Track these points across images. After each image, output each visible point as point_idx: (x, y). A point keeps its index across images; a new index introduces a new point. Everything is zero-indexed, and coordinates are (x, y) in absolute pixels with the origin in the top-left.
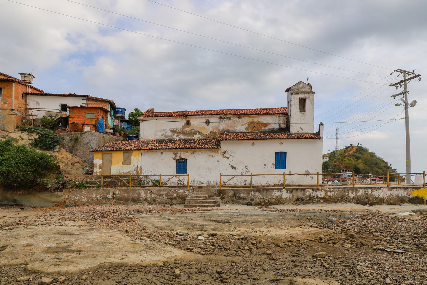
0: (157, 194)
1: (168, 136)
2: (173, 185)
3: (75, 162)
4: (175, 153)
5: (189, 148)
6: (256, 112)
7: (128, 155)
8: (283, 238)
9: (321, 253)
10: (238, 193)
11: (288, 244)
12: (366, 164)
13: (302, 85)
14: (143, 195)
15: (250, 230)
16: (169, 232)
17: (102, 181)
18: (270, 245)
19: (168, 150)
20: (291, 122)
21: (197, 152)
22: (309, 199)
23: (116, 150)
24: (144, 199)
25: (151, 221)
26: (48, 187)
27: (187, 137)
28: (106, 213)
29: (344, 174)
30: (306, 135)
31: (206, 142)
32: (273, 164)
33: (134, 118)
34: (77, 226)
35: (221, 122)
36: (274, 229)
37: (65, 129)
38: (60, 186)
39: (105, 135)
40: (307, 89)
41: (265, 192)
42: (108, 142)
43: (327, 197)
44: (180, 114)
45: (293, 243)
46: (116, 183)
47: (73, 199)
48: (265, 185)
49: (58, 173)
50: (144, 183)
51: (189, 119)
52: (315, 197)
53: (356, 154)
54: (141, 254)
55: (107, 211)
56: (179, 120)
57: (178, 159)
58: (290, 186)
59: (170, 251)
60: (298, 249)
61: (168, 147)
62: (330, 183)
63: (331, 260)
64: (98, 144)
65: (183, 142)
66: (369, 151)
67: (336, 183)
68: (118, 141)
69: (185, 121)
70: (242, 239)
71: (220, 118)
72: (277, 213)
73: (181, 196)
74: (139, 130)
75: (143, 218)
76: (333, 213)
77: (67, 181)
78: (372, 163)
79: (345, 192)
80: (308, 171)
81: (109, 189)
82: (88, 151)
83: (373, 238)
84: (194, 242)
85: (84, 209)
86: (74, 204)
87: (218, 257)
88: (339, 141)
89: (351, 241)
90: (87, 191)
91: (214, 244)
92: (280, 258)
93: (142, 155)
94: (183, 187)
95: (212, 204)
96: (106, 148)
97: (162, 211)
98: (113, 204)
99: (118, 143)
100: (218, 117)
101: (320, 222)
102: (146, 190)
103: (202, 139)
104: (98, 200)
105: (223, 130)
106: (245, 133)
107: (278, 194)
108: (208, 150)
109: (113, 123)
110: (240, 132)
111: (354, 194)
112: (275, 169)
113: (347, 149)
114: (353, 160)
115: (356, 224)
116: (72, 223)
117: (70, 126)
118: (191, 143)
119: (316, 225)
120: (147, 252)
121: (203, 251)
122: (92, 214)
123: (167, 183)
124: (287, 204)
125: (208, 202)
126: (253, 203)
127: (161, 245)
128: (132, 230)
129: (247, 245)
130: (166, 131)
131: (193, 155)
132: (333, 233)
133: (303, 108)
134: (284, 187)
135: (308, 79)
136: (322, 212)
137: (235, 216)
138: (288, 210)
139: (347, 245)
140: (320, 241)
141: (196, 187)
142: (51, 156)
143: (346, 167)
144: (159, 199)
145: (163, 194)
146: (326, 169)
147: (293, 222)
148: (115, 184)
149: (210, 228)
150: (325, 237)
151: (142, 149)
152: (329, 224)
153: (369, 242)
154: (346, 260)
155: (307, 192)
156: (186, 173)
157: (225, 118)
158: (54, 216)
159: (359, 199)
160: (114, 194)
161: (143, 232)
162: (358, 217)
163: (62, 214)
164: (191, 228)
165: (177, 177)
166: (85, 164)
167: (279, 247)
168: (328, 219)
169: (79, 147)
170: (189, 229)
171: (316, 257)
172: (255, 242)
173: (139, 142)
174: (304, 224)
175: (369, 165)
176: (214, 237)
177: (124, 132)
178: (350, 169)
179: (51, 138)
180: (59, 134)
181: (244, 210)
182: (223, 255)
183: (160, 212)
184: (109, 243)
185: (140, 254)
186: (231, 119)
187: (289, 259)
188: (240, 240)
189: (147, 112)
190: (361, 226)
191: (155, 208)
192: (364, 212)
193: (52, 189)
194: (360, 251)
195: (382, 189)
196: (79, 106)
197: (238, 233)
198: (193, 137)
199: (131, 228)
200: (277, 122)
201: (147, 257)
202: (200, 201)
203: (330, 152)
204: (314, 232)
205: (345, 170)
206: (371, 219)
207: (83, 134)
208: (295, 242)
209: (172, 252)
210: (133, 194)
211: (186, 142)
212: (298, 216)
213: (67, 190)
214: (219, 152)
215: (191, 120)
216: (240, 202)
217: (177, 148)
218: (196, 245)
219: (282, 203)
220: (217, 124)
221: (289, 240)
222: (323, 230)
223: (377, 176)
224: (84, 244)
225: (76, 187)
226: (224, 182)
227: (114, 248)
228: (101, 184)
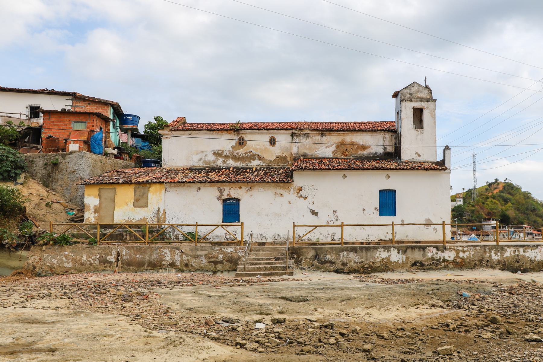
0: (190, 256)
1: (210, 161)
2: (217, 240)
3: (52, 201)
4: (221, 190)
5: (243, 182)
6: (349, 126)
7: (143, 191)
8: (390, 324)
9: (446, 347)
10: (322, 253)
11: (397, 334)
12: (518, 209)
13: (416, 88)
14: (168, 257)
15: (338, 312)
16: (208, 316)
17: (99, 234)
18: (368, 335)
19: (209, 184)
20: (402, 144)
21: (256, 188)
22: (431, 262)
23: (123, 183)
24: (170, 263)
25: (179, 299)
26: (4, 242)
27: (240, 164)
28: (103, 286)
29: (487, 225)
30: (425, 163)
31: (271, 173)
32: (376, 208)
33: (153, 132)
34: (52, 308)
35: (294, 141)
36: (376, 310)
37: (36, 147)
38: (25, 241)
39: (103, 158)
40: (424, 94)
41: (364, 251)
42: (110, 169)
43: (459, 260)
44: (228, 127)
45: (405, 332)
46: (123, 237)
47: (48, 262)
48: (364, 241)
49: (23, 220)
50: (170, 237)
51: (244, 136)
52: (441, 260)
53: (503, 194)
54: (159, 354)
55: (107, 282)
56: (226, 136)
57: (226, 199)
58: (403, 243)
59: (208, 348)
60: (413, 341)
61: (209, 180)
62: (465, 238)
63: (461, 358)
64: (92, 173)
65: (234, 172)
66: (523, 190)
67: (474, 238)
68: (127, 168)
69: (237, 138)
70: (326, 327)
71: (293, 135)
72: (382, 284)
73: (230, 258)
74: (161, 152)
75: (167, 293)
76: (467, 285)
77: (37, 234)
78: (527, 209)
79: (485, 251)
80: (429, 220)
81: (111, 246)
82: (75, 183)
83: (526, 323)
84: (249, 333)
85: (68, 280)
86: (50, 272)
87: (285, 356)
88: (478, 174)
89: (492, 328)
90: (73, 249)
91: (281, 336)
92: (384, 356)
93: (166, 191)
94: (235, 243)
95: (281, 271)
96: (106, 179)
97: (198, 283)
98: (117, 271)
99: (126, 171)
100: (288, 134)
101: (447, 299)
102: (173, 248)
103: (264, 168)
104: (91, 264)
105: (298, 153)
106: (332, 159)
107: (384, 255)
108: (274, 184)
109: (118, 139)
110: (324, 158)
111: (498, 256)
112: (380, 215)
113: (489, 187)
114: (499, 204)
115: (501, 301)
116: (44, 302)
117: (44, 142)
118: (246, 173)
119: (442, 304)
120: (169, 350)
121: (263, 348)
122: (81, 287)
123: (208, 237)
124: (398, 270)
125: (274, 268)
126: (346, 269)
127: (193, 338)
128: (146, 314)
129: (334, 337)
130: (205, 153)
131: (250, 193)
132: (467, 315)
133: (419, 122)
134: (394, 244)
135: (426, 79)
136: (451, 283)
137: (315, 289)
138: (399, 280)
139: (486, 335)
140: (446, 329)
141: (254, 244)
142: (10, 191)
143: (489, 214)
144: (194, 262)
145: (201, 254)
146: (460, 217)
147: (406, 299)
148: (120, 239)
149: (275, 310)
150: (453, 323)
151: (166, 182)
152: (460, 302)
153: (519, 329)
154: (483, 358)
155: (428, 253)
156: (239, 221)
157: (300, 136)
158: (13, 292)
159: (507, 263)
160: (118, 254)
161: (165, 317)
162: (504, 291)
163: (28, 289)
164: (244, 310)
165: (225, 227)
166: (70, 205)
167: (383, 338)
168: (460, 294)
169: (59, 176)
170: (241, 311)
171: (439, 354)
172: (345, 332)
173: (161, 171)
174: (422, 302)
175: (523, 212)
176: (282, 325)
177: (137, 154)
178: (495, 216)
179: (12, 162)
180: (25, 155)
181: (331, 281)
182: (295, 353)
183: (195, 284)
184: (106, 337)
185: (157, 354)
186: (310, 138)
187: (397, 357)
188: (323, 329)
189: (174, 122)
190: (508, 305)
191: (188, 278)
192: (513, 282)
193: (11, 246)
194: (505, 343)
195: (539, 247)
196: (60, 110)
197: (321, 317)
198: (249, 164)
199: (146, 311)
200: (381, 143)
201: (168, 358)
202: (261, 266)
203: (465, 191)
204: (437, 315)
205: (488, 219)
206: (523, 293)
207: (67, 156)
208: (408, 331)
209: (211, 349)
210: (151, 255)
211: (238, 171)
212: (413, 290)
213: (38, 247)
214: (291, 188)
215: (246, 138)
216: (326, 268)
217: (223, 182)
218: (252, 337)
219: (392, 270)
220: (287, 145)
221: (399, 327)
222: (451, 311)
223: (535, 228)
224: (61, 338)
225: (54, 242)
226: (300, 237)
227: (112, 345)
228: (96, 238)
